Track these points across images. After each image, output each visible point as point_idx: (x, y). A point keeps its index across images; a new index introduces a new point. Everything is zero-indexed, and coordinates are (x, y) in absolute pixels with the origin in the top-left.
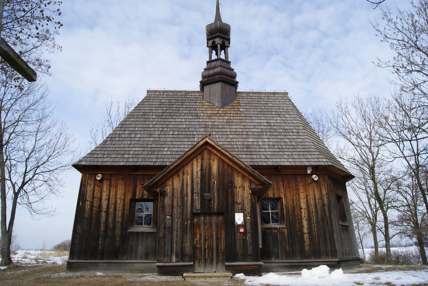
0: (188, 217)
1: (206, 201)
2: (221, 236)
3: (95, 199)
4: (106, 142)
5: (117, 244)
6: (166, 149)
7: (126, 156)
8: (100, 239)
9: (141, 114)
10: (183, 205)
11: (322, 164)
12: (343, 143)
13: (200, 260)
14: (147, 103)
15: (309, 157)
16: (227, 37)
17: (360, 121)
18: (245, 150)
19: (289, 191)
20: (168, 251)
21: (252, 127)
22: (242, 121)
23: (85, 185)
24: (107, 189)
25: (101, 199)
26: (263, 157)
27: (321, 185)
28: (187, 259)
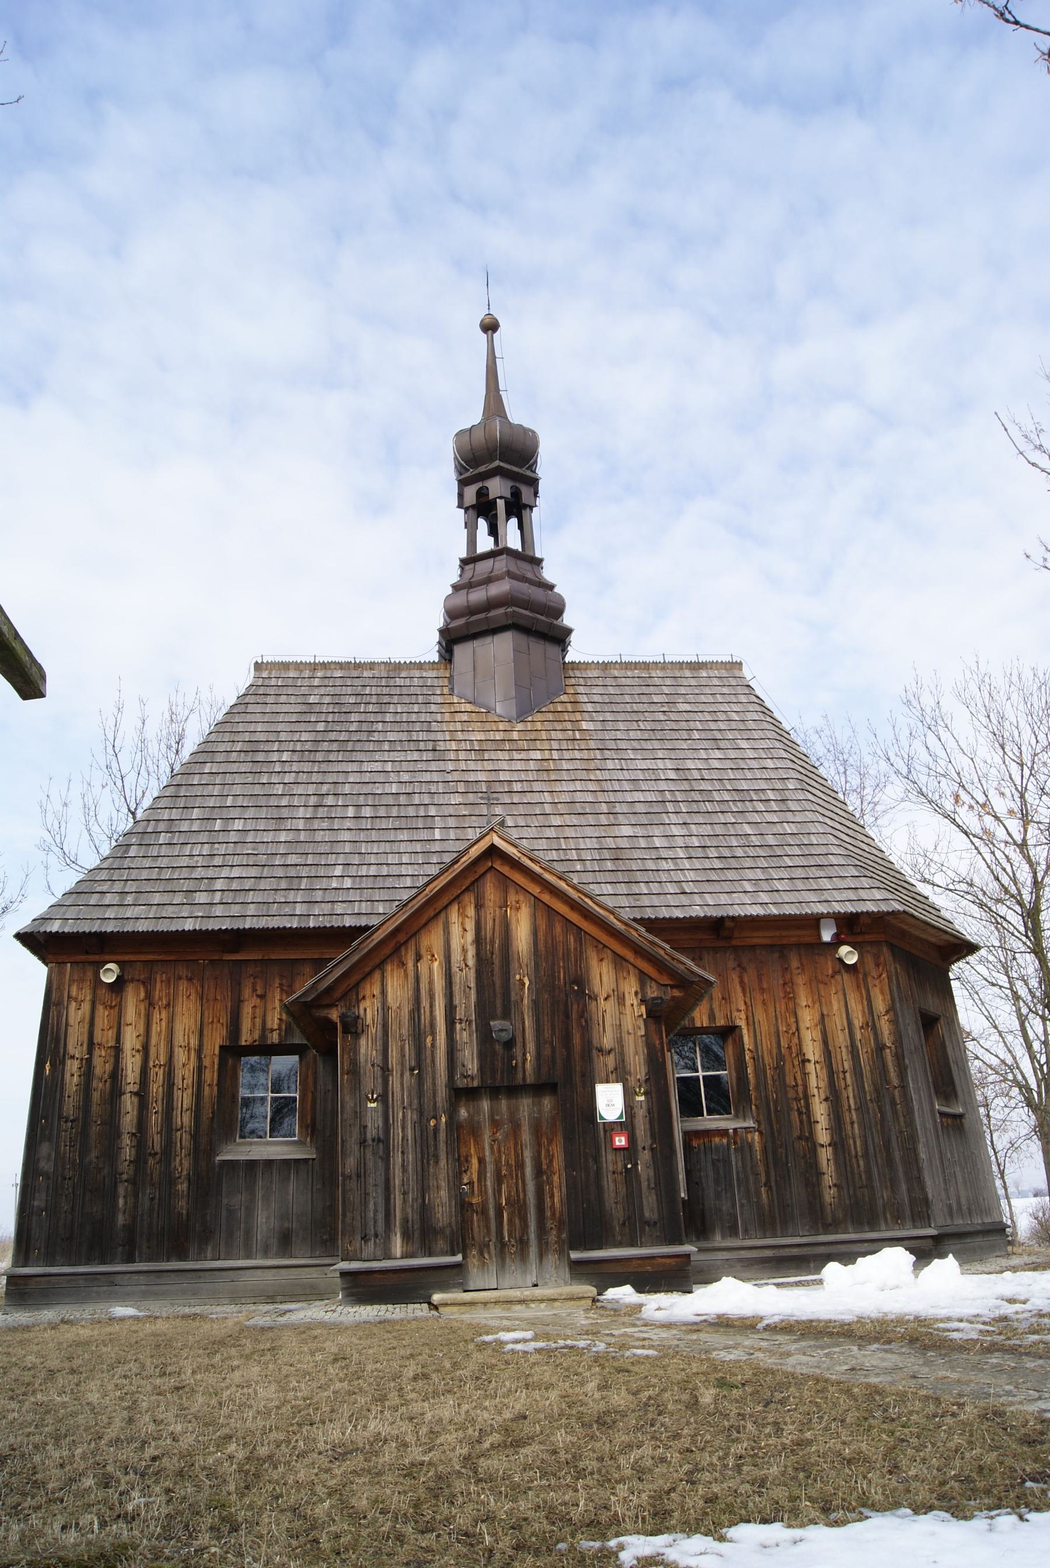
0: (439, 1104)
1: (498, 1048)
2: (551, 1161)
3: (96, 1052)
4: (127, 851)
5: (182, 1205)
6: (338, 871)
7: (202, 898)
8: (121, 1191)
9: (238, 747)
10: (420, 1064)
11: (871, 907)
12: (930, 828)
13: (483, 1249)
14: (259, 708)
15: (826, 884)
16: (529, 473)
17: (987, 752)
18: (609, 865)
19: (764, 1003)
20: (375, 1222)
21: (627, 786)
22: (592, 765)
23: (59, 1004)
24: (138, 1014)
25: (117, 1050)
26: (671, 888)
27: (869, 979)
28: (441, 1244)
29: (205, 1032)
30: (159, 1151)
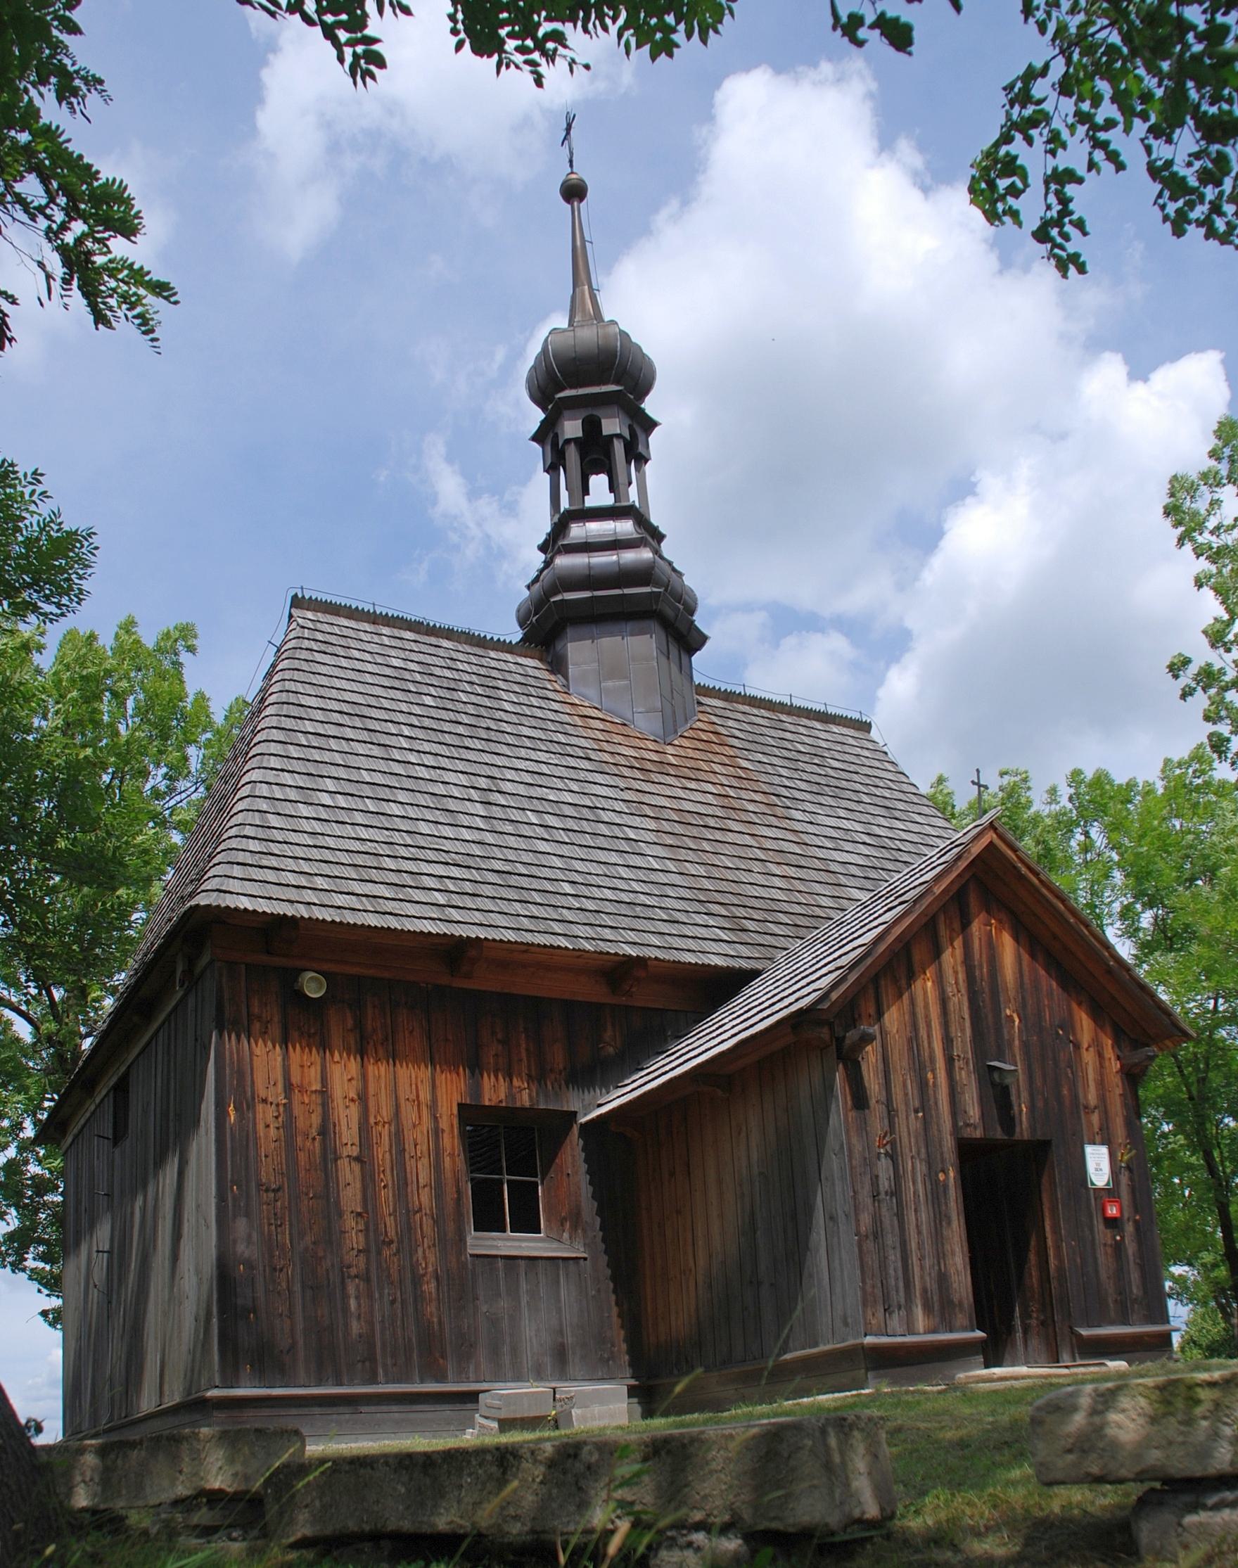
3: (296, 1096)
8: (351, 1290)
29: (438, 1082)
30: (395, 1238)
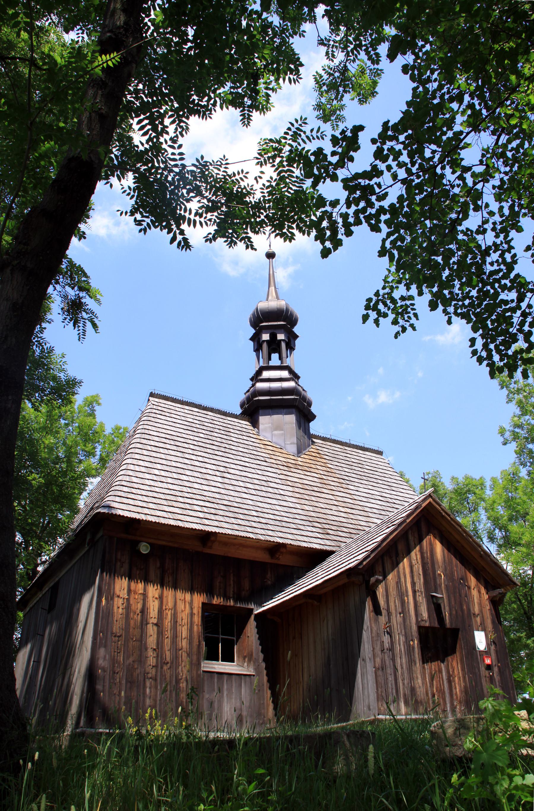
2: (453, 670)
8: (148, 684)
